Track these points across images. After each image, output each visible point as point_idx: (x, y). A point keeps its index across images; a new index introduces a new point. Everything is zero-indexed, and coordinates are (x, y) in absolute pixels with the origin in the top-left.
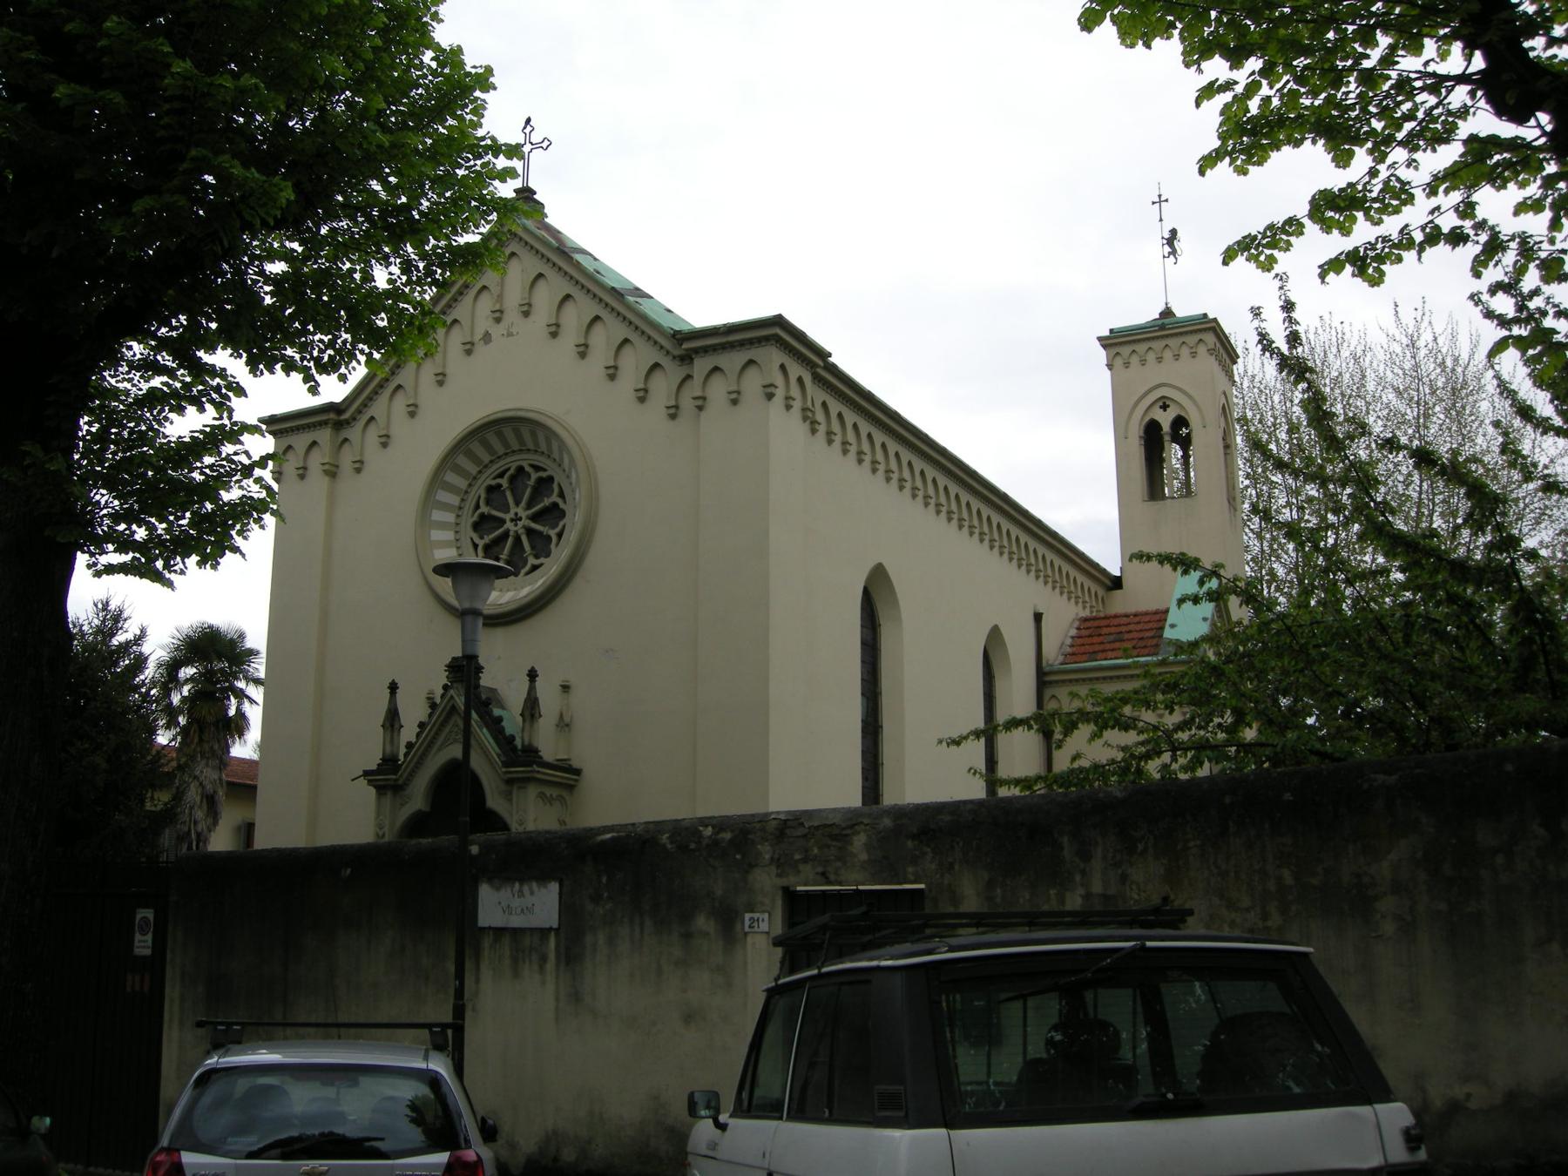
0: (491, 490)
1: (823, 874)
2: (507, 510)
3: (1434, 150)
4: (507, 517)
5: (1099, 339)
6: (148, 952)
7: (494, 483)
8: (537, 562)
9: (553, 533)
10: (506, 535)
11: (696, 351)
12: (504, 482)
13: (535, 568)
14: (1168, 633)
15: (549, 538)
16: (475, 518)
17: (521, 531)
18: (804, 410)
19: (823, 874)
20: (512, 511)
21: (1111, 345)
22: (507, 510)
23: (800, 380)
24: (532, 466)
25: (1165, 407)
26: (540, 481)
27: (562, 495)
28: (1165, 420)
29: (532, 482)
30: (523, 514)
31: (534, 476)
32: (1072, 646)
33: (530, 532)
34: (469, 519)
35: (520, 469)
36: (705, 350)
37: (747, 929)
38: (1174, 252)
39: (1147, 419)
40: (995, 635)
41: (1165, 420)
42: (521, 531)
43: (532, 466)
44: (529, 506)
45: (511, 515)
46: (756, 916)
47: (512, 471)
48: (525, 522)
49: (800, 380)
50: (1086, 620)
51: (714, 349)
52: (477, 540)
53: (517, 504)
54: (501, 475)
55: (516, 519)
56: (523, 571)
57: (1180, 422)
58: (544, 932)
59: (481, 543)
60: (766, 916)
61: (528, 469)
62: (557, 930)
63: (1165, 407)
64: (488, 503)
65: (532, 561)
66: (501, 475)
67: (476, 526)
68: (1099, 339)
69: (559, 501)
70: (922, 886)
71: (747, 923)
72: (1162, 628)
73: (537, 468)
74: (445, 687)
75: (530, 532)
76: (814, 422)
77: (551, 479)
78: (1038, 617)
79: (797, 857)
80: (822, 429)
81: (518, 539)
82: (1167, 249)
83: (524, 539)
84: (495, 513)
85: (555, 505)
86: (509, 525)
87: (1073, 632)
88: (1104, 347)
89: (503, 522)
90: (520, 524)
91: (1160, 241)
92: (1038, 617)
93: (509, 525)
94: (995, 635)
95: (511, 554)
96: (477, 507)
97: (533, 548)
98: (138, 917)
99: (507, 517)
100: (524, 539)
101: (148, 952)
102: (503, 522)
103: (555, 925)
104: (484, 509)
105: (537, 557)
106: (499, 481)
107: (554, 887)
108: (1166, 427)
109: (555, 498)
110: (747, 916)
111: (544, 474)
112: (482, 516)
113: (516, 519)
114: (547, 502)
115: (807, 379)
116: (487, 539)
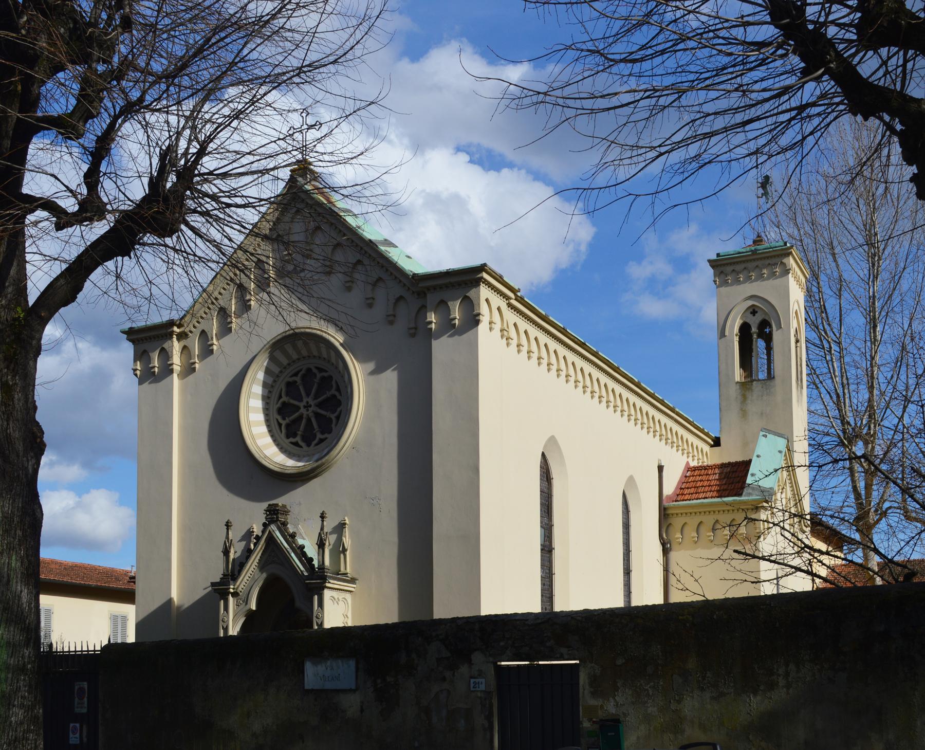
0: (289, 384)
2: (301, 400)
3: (718, 255)
4: (301, 405)
5: (709, 261)
6: (85, 711)
7: (291, 380)
8: (322, 437)
9: (333, 416)
10: (300, 418)
11: (428, 289)
12: (298, 379)
13: (321, 441)
15: (331, 420)
16: (279, 405)
17: (305, 416)
20: (305, 400)
21: (717, 266)
23: (499, 309)
24: (317, 368)
25: (754, 313)
26: (323, 379)
27: (338, 389)
29: (317, 380)
30: (312, 403)
31: (319, 376)
33: (317, 415)
34: (275, 407)
35: (309, 370)
38: (766, 194)
40: (631, 480)
42: (311, 415)
43: (317, 368)
44: (316, 398)
45: (304, 403)
46: (477, 680)
47: (303, 372)
49: (499, 309)
50: (695, 469)
52: (281, 421)
53: (308, 395)
54: (296, 374)
59: (284, 423)
61: (314, 370)
64: (287, 395)
65: (319, 436)
66: (296, 374)
68: (709, 261)
69: (337, 394)
70: (578, 662)
71: (472, 685)
73: (320, 370)
74: (265, 525)
75: (317, 415)
78: (661, 468)
80: (514, 343)
81: (309, 420)
82: (761, 191)
83: (313, 420)
84: (292, 401)
85: (334, 396)
86: (302, 410)
88: (713, 267)
89: (298, 408)
90: (311, 409)
91: (755, 185)
92: (661, 468)
94: (631, 480)
96: (280, 397)
97: (319, 426)
98: (76, 688)
99: (301, 405)
100: (313, 420)
101: (85, 711)
102: (298, 408)
105: (323, 433)
106: (295, 378)
109: (333, 392)
111: (325, 374)
112: (284, 404)
113: (307, 406)
114: (328, 394)
115: (503, 304)
116: (287, 421)
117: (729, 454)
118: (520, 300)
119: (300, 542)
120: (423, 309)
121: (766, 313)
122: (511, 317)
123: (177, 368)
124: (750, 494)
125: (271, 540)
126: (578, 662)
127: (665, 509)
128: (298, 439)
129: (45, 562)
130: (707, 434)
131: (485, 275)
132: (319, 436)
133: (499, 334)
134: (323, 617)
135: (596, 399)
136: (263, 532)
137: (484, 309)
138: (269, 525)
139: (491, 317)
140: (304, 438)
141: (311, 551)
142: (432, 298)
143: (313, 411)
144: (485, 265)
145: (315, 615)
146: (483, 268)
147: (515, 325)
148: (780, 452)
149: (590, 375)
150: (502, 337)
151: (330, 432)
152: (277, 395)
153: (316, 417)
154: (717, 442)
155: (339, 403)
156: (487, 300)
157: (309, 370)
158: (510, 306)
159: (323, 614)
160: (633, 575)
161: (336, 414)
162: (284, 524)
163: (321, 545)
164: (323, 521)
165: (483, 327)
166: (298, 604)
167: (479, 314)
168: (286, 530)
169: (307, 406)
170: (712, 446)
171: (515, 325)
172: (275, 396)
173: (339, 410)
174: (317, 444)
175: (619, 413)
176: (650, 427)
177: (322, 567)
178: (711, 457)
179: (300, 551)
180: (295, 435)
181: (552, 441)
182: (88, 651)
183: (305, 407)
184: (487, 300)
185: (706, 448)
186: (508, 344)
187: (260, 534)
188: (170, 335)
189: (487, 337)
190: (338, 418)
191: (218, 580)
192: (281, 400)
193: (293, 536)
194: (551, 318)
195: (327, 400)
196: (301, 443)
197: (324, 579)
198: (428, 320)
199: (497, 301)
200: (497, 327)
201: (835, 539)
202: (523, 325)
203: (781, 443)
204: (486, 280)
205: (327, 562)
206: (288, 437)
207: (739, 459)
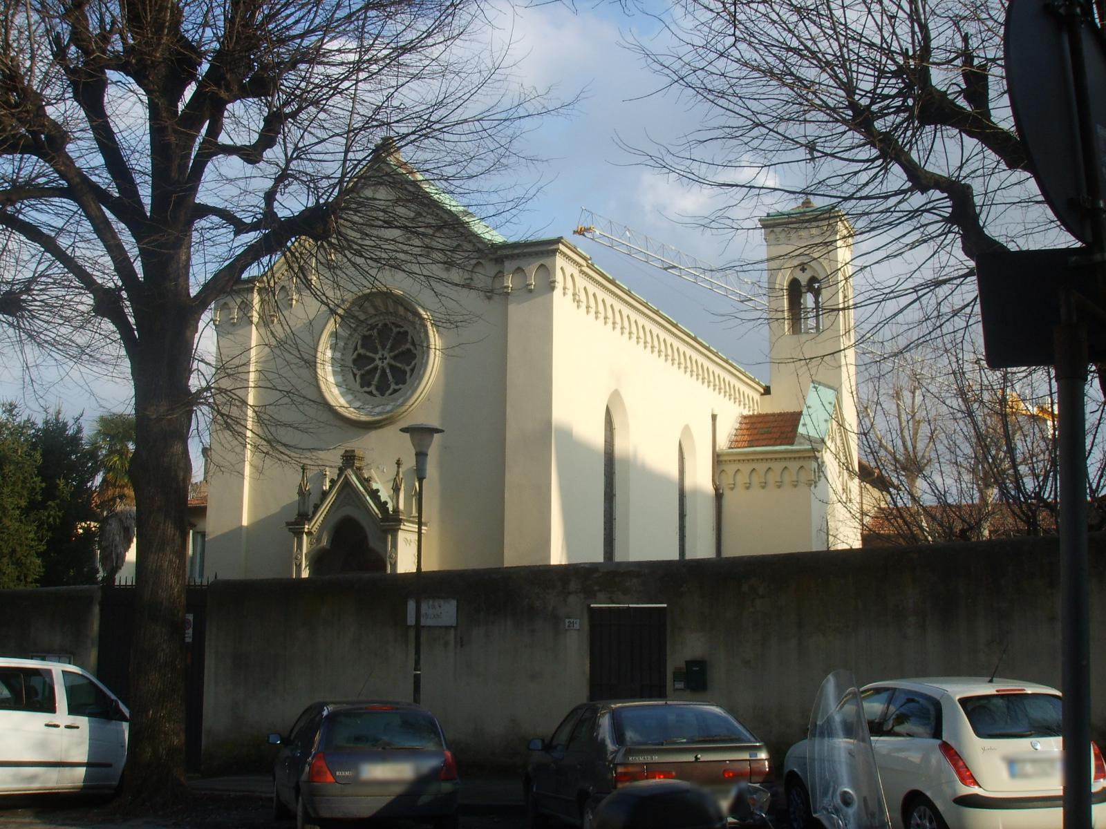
1: (610, 598)
4: (377, 357)
8: (397, 387)
9: (408, 369)
10: (376, 368)
11: (507, 257)
13: (395, 391)
14: (801, 430)
16: (355, 356)
18: (574, 295)
19: (610, 598)
22: (376, 352)
23: (572, 276)
28: (803, 278)
30: (386, 355)
32: (735, 435)
34: (350, 357)
36: (512, 257)
37: (567, 627)
39: (791, 278)
40: (687, 429)
41: (803, 278)
43: (393, 324)
45: (380, 355)
48: (377, 357)
49: (572, 276)
51: (518, 256)
55: (383, 359)
56: (387, 393)
57: (813, 280)
58: (447, 628)
60: (578, 621)
62: (455, 628)
63: (803, 270)
65: (393, 386)
67: (355, 361)
69: (412, 348)
70: (665, 605)
71: (567, 624)
72: (797, 426)
75: (392, 367)
76: (578, 301)
77: (406, 333)
78: (714, 417)
79: (596, 588)
81: (383, 371)
86: (378, 362)
87: (737, 426)
89: (374, 360)
90: (386, 362)
92: (714, 417)
93: (378, 362)
94: (687, 429)
95: (379, 381)
96: (356, 349)
100: (388, 371)
102: (374, 360)
103: (455, 625)
104: (361, 351)
105: (397, 384)
107: (454, 603)
108: (804, 283)
109: (408, 346)
110: (567, 620)
112: (359, 355)
113: (383, 359)
114: (404, 348)
115: (576, 273)
117: (775, 405)
118: (591, 267)
119: (374, 486)
120: (500, 274)
121: (815, 271)
122: (581, 282)
123: (255, 319)
124: (801, 444)
125: (347, 483)
126: (665, 605)
127: (718, 456)
128: (373, 389)
129: (569, 557)
130: (758, 384)
131: (561, 247)
132: (393, 386)
133: (572, 297)
134: (396, 557)
135: (656, 353)
136: (339, 476)
137: (559, 276)
138: (346, 470)
139: (638, 333)
140: (378, 389)
141: (384, 495)
142: (509, 265)
143: (388, 364)
144: (561, 238)
145: (388, 554)
146: (558, 241)
147: (585, 289)
148: (830, 403)
149: (594, 295)
150: (574, 300)
151: (404, 382)
152: (353, 347)
153: (390, 369)
154: (767, 391)
155: (414, 357)
156: (562, 268)
157: (385, 325)
158: (581, 271)
159: (396, 554)
160: (688, 519)
161: (410, 367)
162: (359, 469)
163: (396, 489)
164: (398, 467)
165: (557, 293)
166: (373, 543)
167: (554, 282)
168: (362, 474)
169: (382, 359)
170: (762, 394)
171: (585, 289)
172: (351, 347)
173: (413, 363)
174: (391, 394)
175: (676, 365)
176: (705, 378)
177: (396, 510)
178: (757, 405)
179: (374, 494)
180: (369, 385)
181: (616, 395)
182: (201, 585)
183: (380, 359)
184: (562, 268)
185: (757, 397)
186: (578, 307)
187: (336, 478)
188: (252, 290)
189: (561, 302)
190: (412, 370)
191: (293, 520)
192: (356, 353)
193: (368, 480)
194: (617, 282)
195: (403, 353)
196: (375, 392)
197: (400, 521)
198: (505, 285)
199: (571, 269)
200: (570, 292)
201: (882, 484)
202: (592, 288)
203: (828, 395)
204: (561, 251)
205: (401, 506)
206: (362, 386)
207: (792, 410)
